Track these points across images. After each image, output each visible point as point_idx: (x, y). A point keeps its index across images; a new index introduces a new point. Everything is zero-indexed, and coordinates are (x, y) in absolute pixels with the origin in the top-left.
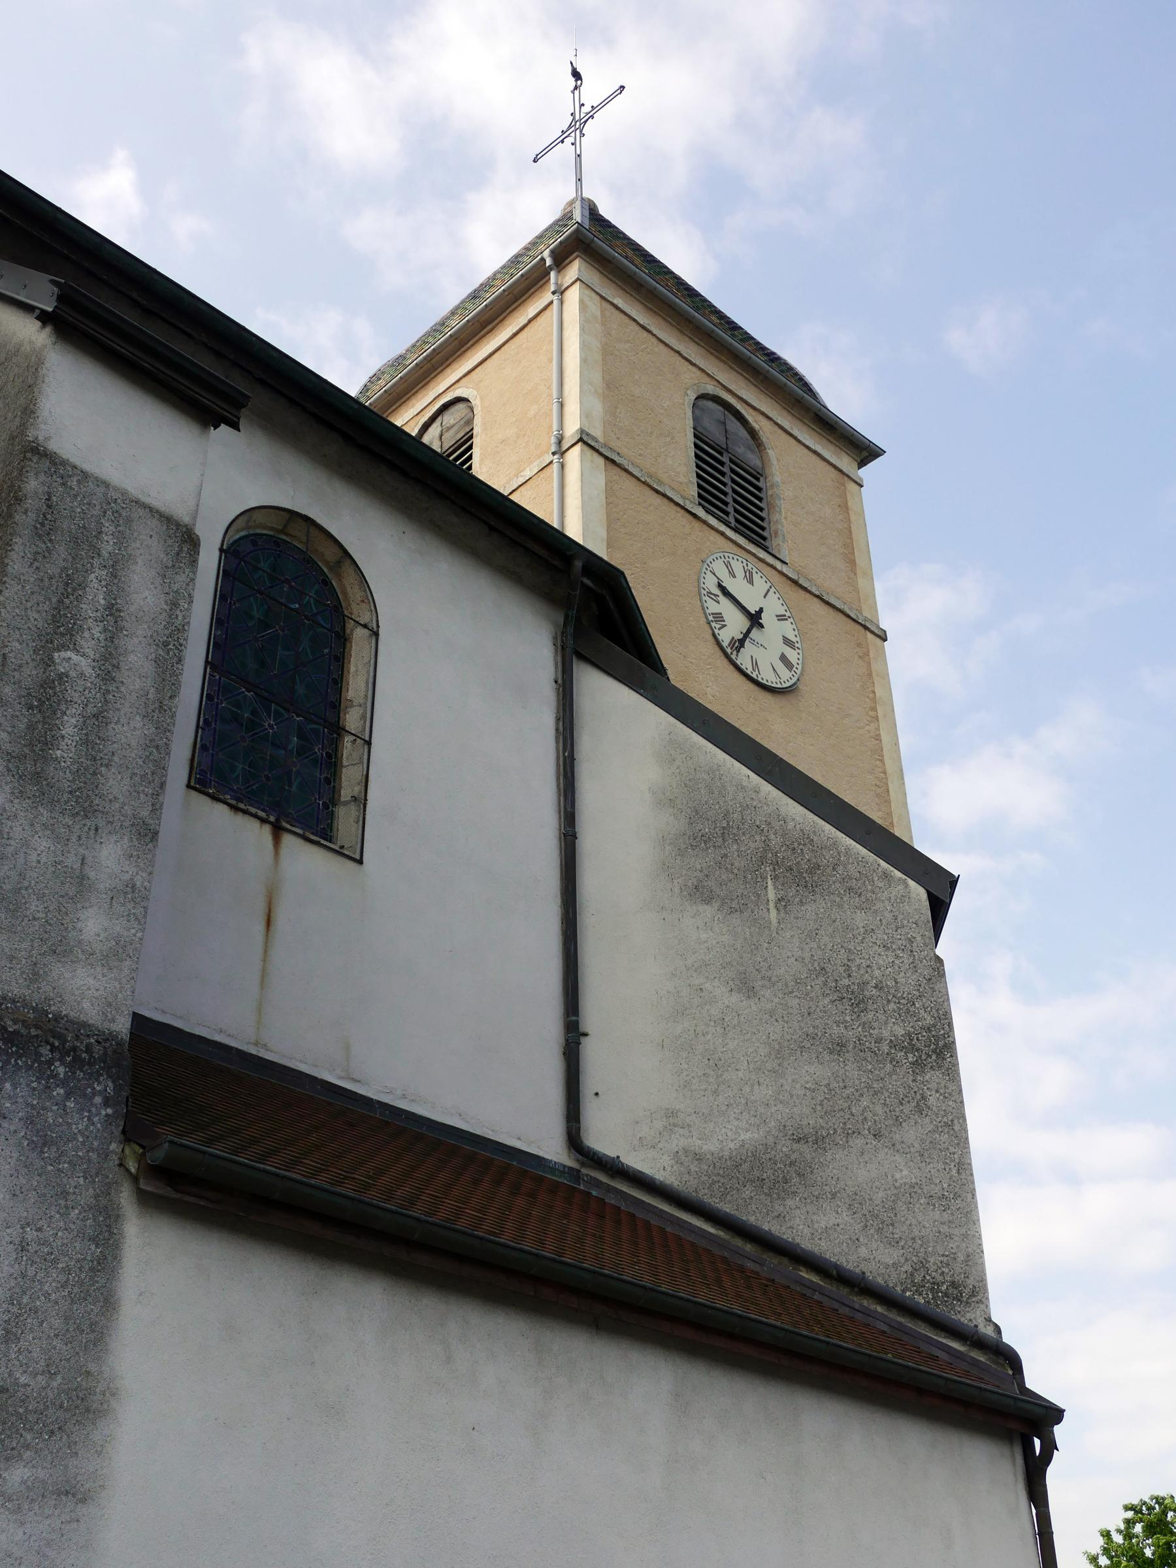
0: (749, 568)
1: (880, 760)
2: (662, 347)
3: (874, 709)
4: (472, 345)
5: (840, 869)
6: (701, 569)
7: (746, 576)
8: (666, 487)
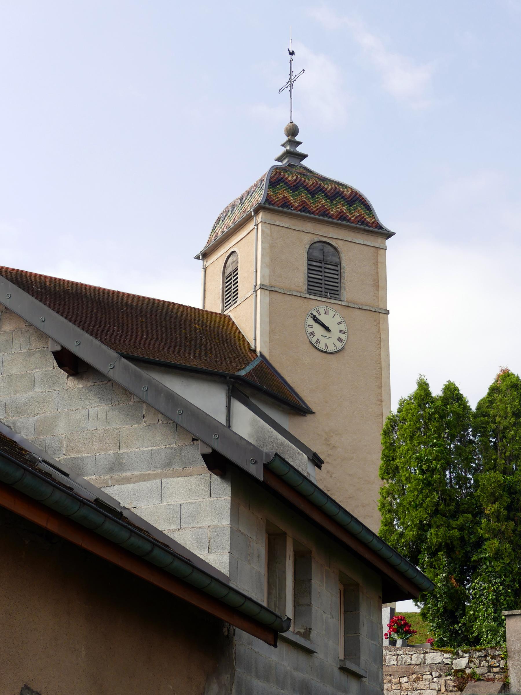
0: (327, 309)
1: (379, 364)
2: (296, 232)
3: (379, 344)
4: (238, 231)
5: (289, 452)
6: (306, 318)
7: (325, 312)
8: (294, 292)
